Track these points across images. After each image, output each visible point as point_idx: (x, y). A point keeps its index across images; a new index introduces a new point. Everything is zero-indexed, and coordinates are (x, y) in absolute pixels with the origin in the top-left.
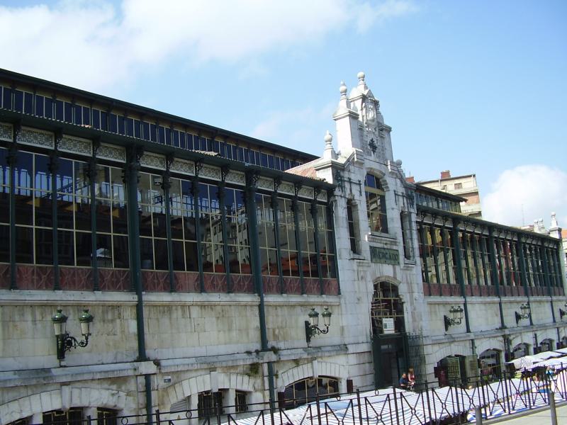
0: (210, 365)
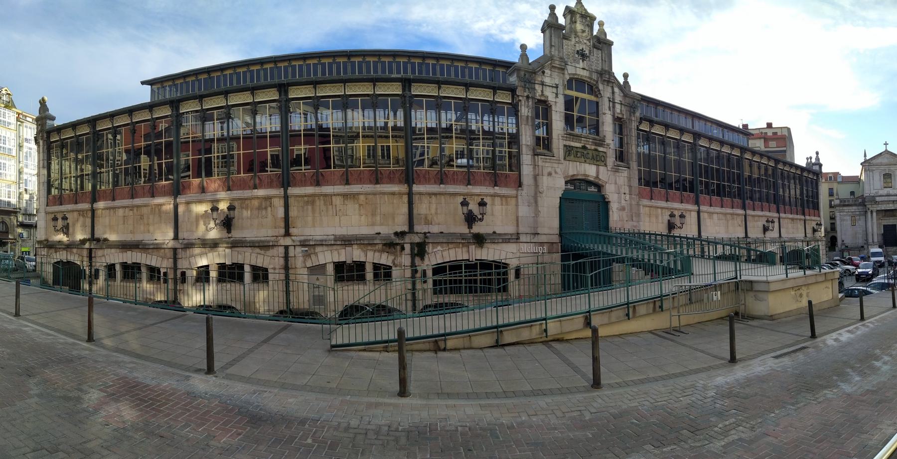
0: (346, 241)
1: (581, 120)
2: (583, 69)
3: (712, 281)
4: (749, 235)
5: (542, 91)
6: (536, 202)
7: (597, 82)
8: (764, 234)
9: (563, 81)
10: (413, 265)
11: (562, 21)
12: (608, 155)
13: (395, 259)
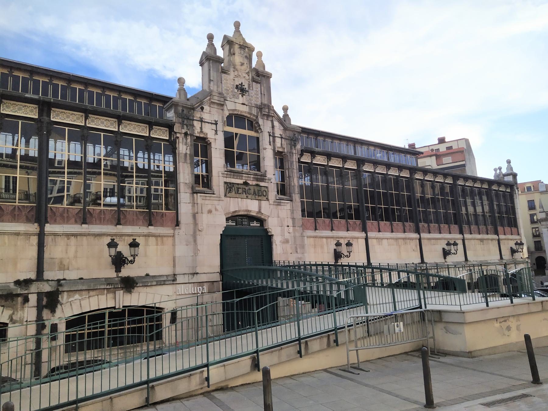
1: (240, 157)
2: (243, 104)
3: (391, 311)
4: (426, 260)
5: (201, 128)
6: (195, 241)
7: (257, 117)
8: (445, 258)
9: (223, 117)
10: (39, 317)
11: (220, 53)
12: (270, 190)
13: (13, 313)
